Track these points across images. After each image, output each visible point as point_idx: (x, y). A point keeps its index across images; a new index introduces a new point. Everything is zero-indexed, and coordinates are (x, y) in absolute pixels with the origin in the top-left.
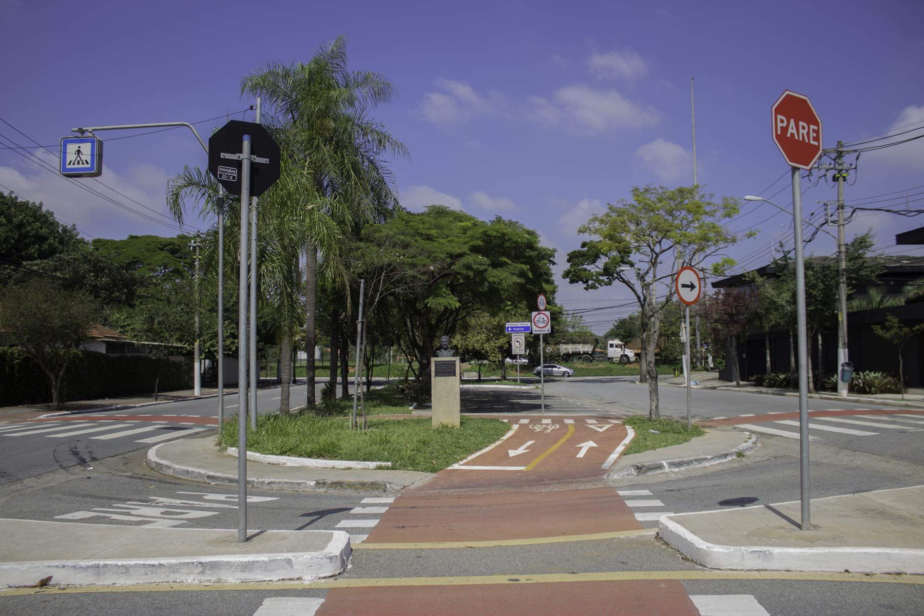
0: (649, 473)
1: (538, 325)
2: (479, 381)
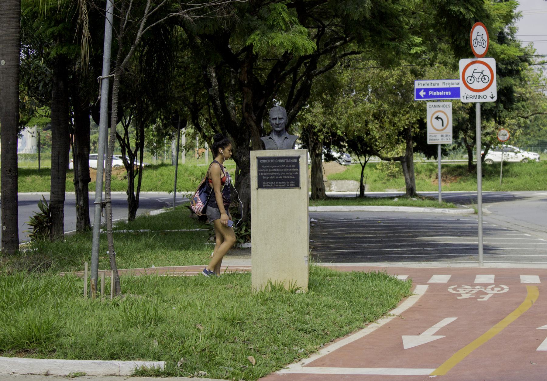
1: (471, 86)
2: (362, 198)
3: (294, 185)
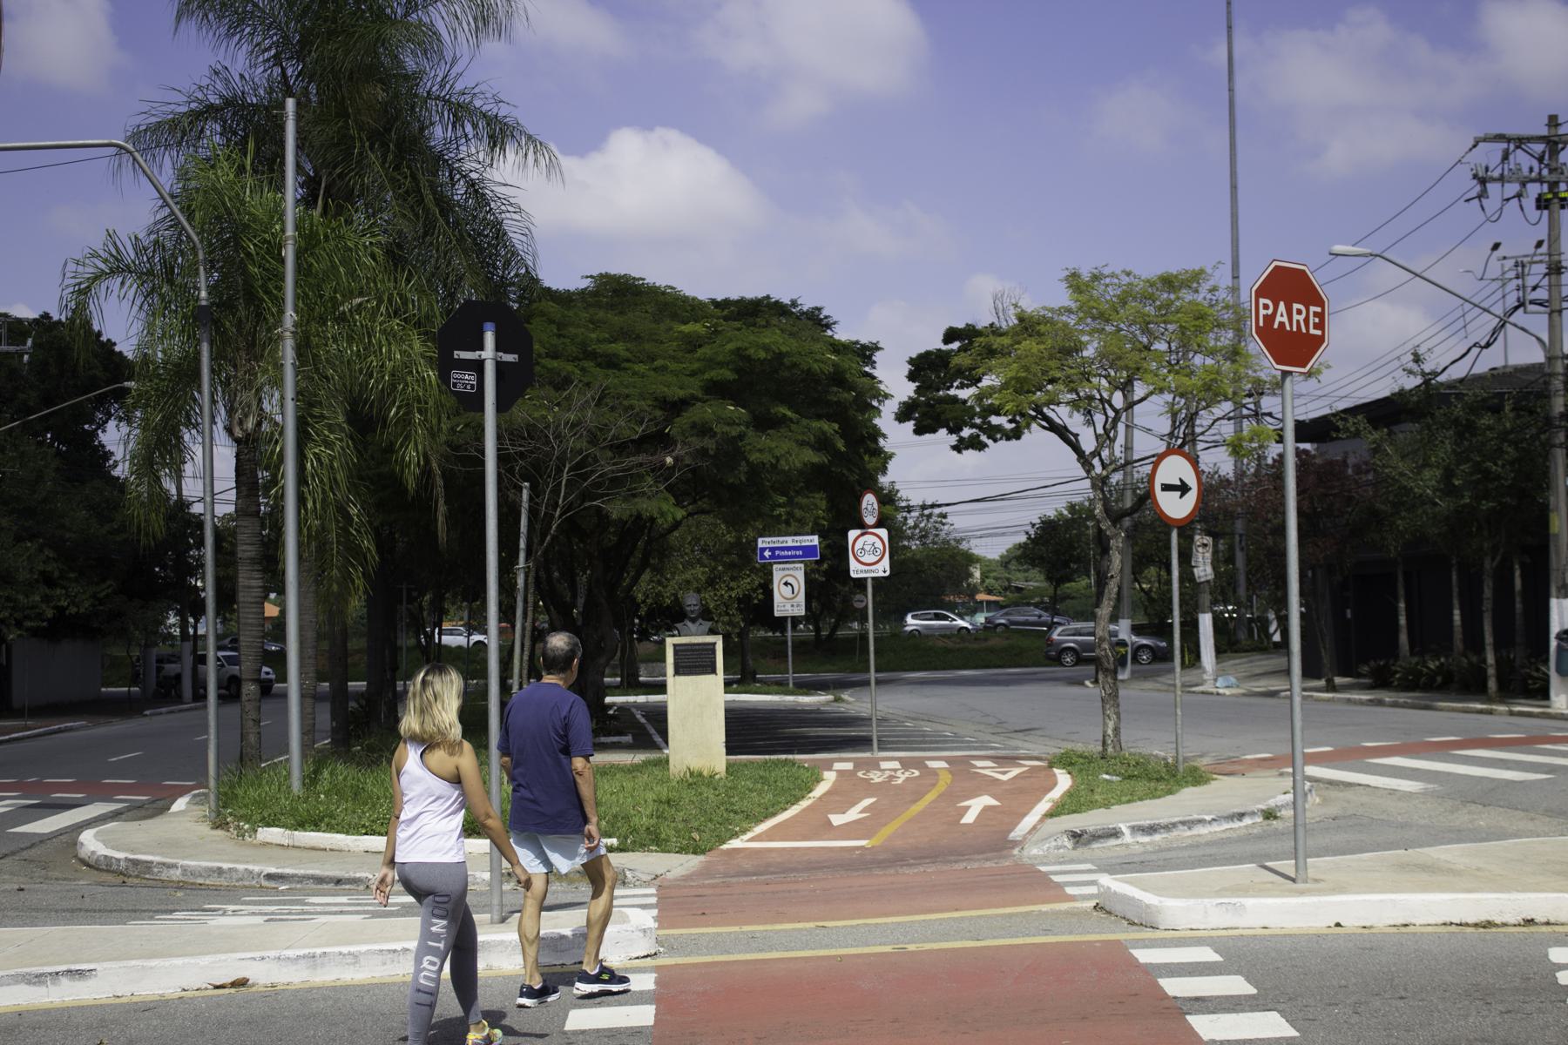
0: (1095, 845)
1: (861, 559)
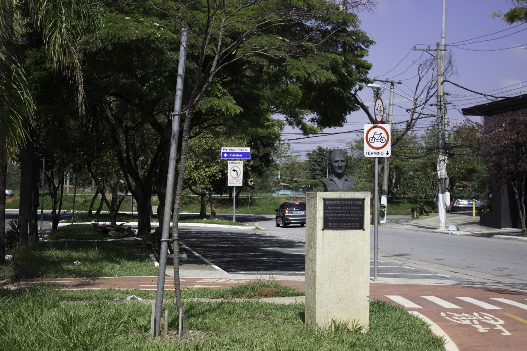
3: (358, 226)
